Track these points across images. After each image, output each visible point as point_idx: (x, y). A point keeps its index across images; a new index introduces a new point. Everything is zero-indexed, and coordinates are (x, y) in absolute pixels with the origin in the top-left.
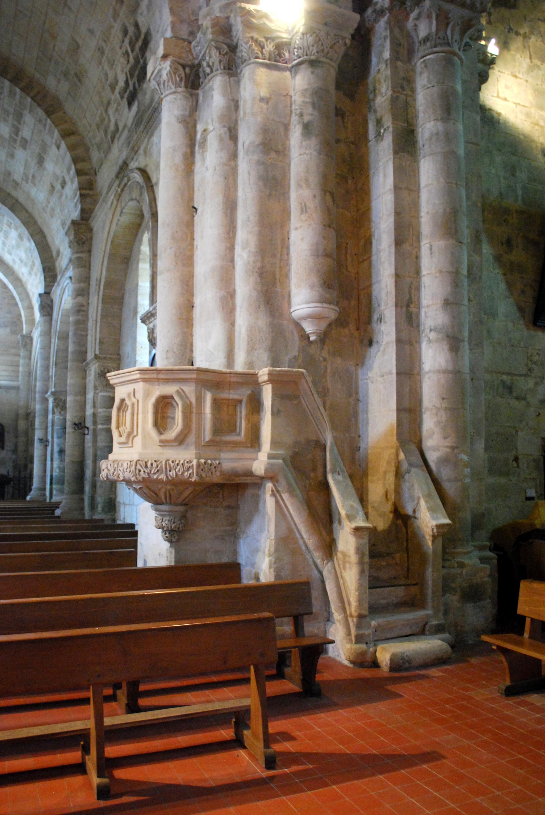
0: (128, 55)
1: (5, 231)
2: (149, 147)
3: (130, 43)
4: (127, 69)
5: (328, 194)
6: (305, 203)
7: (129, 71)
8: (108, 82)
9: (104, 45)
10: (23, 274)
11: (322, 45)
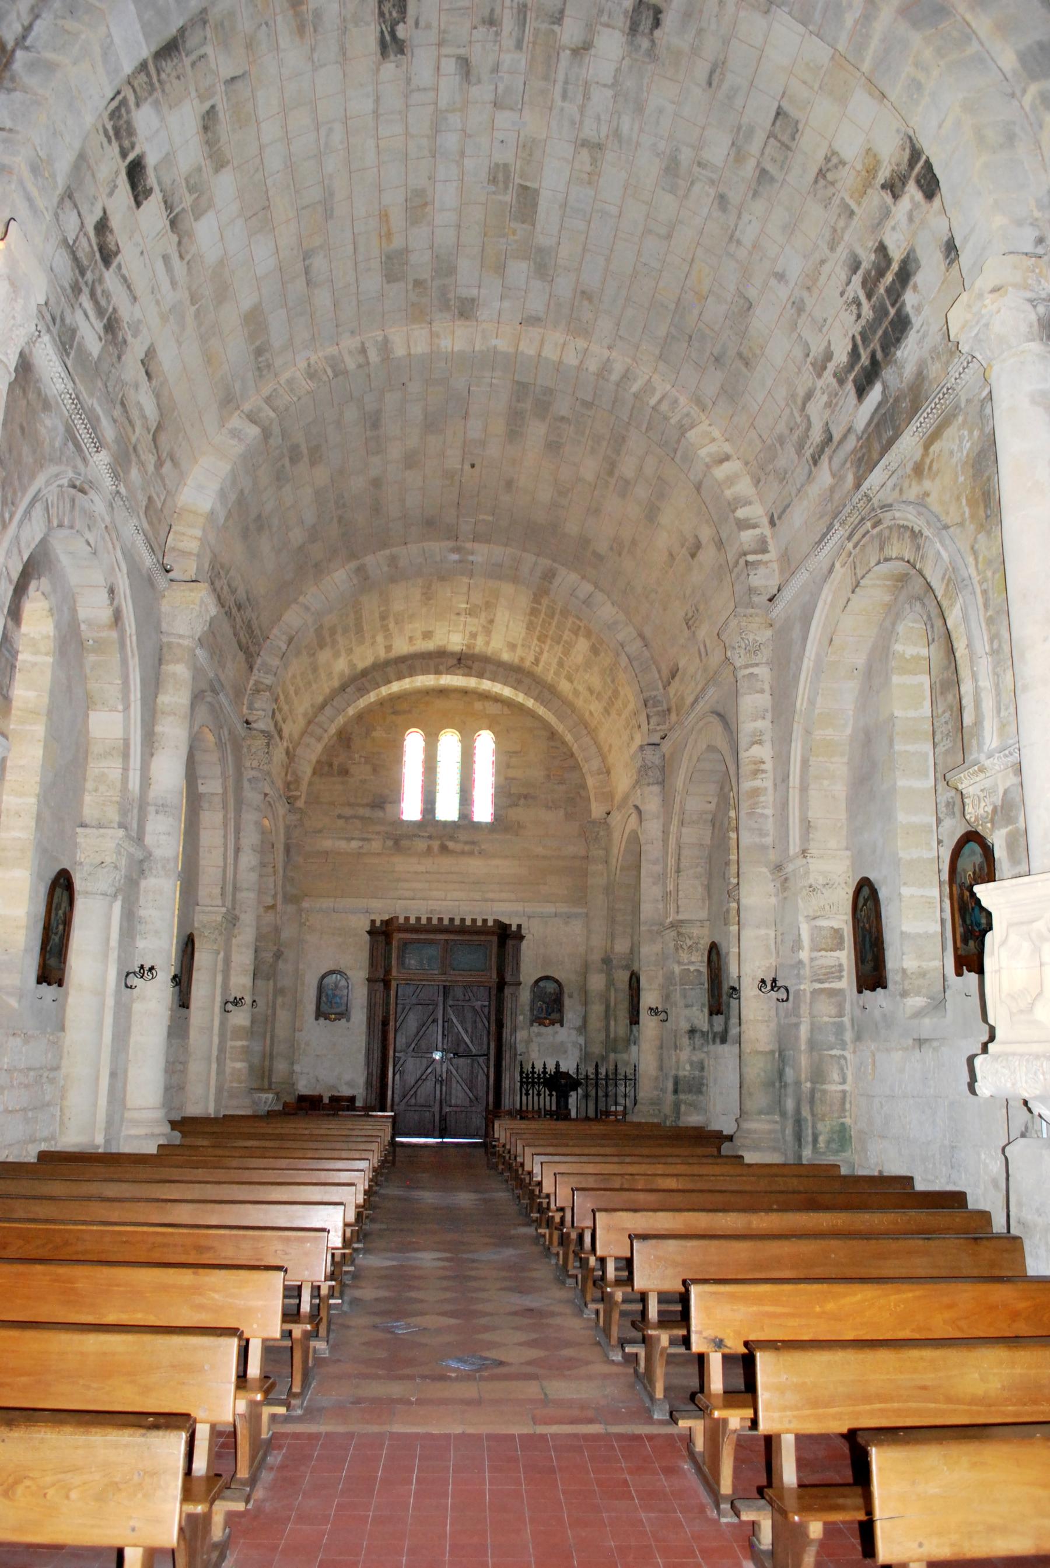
0: (859, 305)
1: (566, 642)
2: (928, 461)
3: (864, 284)
4: (856, 329)
7: (861, 333)
8: (809, 360)
9: (805, 294)
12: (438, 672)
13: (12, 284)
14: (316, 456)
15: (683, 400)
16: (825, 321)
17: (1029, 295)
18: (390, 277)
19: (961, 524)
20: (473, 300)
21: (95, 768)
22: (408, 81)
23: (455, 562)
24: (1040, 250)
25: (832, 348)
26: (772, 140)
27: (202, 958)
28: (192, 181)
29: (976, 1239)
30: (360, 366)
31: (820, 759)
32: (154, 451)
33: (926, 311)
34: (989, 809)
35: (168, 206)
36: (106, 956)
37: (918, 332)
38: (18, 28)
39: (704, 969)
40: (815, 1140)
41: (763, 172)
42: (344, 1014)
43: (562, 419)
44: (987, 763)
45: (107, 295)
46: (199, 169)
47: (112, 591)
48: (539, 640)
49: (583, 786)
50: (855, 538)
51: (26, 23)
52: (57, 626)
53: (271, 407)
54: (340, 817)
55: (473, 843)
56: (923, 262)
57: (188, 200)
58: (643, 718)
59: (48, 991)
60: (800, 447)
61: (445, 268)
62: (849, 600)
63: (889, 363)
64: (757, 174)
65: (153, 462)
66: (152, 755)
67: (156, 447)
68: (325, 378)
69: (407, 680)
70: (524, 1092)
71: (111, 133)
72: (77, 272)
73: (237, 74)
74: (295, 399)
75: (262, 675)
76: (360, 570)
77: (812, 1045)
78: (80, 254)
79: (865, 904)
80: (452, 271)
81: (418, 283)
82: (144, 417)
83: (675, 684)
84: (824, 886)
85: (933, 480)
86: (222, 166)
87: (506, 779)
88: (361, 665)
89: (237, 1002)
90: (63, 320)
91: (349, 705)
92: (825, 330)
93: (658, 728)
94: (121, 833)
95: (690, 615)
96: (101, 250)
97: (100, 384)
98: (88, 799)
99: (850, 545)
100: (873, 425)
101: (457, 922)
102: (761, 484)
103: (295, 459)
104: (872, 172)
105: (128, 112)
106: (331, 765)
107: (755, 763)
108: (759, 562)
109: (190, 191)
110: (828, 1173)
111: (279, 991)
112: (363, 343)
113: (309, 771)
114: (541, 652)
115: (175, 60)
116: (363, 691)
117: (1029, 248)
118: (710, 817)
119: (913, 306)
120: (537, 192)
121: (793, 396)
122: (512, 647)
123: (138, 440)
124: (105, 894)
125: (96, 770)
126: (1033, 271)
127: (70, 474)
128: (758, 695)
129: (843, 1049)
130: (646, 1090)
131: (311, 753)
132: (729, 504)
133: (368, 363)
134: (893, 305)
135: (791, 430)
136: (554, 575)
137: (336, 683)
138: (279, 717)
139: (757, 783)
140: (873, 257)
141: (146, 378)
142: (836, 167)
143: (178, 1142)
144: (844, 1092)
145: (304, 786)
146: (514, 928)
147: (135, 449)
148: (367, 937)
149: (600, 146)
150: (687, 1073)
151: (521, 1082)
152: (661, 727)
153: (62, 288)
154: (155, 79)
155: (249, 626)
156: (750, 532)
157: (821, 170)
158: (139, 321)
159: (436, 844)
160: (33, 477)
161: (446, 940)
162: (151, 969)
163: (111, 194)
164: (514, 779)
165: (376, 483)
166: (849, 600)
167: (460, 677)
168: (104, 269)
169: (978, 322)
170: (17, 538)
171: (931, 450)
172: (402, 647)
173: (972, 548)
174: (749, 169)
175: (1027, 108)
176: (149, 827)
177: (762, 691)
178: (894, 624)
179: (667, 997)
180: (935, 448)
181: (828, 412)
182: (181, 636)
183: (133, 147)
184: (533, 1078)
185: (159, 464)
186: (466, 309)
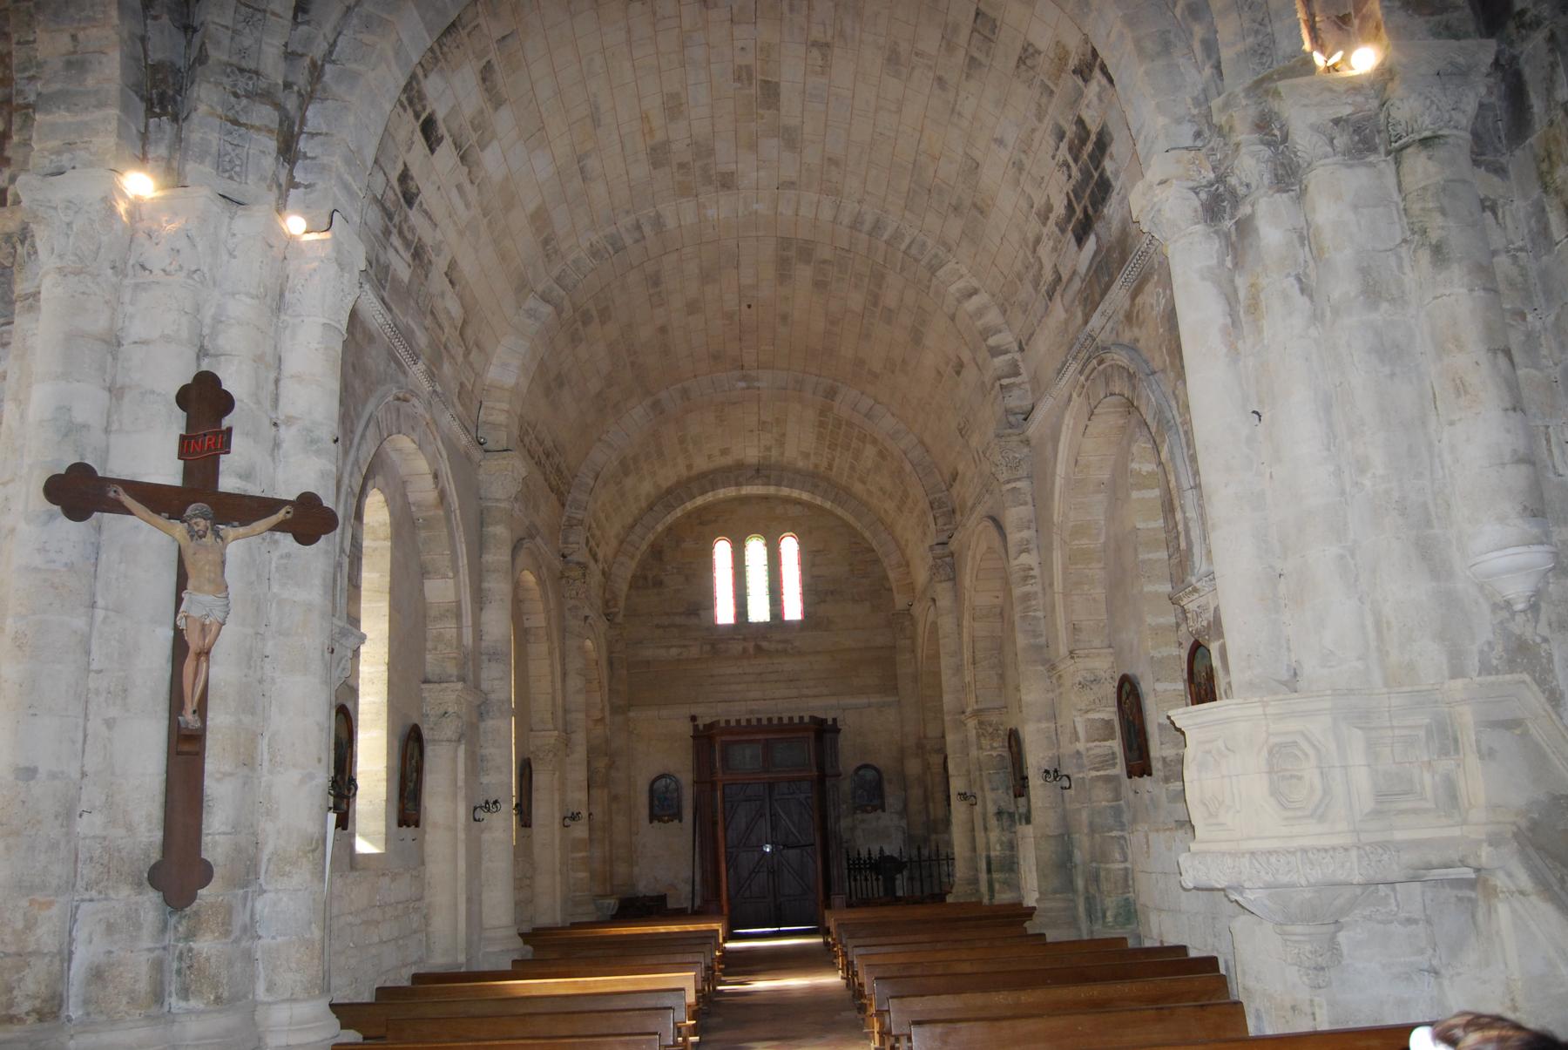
0: (1069, 167)
3: (1070, 149)
4: (1069, 187)
5: (1500, 356)
6: (1461, 378)
7: (1073, 191)
8: (1034, 210)
9: (1023, 156)
10: (886, 511)
11: (1438, 109)
12: (738, 484)
13: (339, 265)
14: (605, 315)
15: (930, 243)
16: (1042, 178)
17: (1192, 184)
18: (656, 164)
19: (1164, 371)
20: (733, 173)
21: (433, 629)
22: (654, 14)
23: (743, 389)
24: (1199, 143)
25: (1052, 201)
26: (975, 34)
27: (541, 779)
28: (476, 122)
29: (1202, 1006)
30: (637, 241)
31: (1079, 566)
32: (462, 344)
33: (1122, 176)
34: (1205, 623)
35: (457, 146)
36: (455, 796)
37: (1118, 194)
38: (325, 46)
39: (1006, 754)
40: (1104, 916)
41: (972, 59)
42: (678, 816)
43: (825, 262)
44: (1198, 585)
45: (412, 229)
46: (481, 112)
47: (436, 476)
48: (829, 448)
49: (886, 578)
50: (1087, 372)
51: (331, 41)
52: (392, 514)
53: (561, 286)
54: (658, 626)
55: (786, 641)
56: (1115, 136)
57: (474, 137)
58: (931, 518)
59: (408, 832)
60: (1036, 285)
61: (703, 150)
62: (1087, 426)
63: (1099, 218)
64: (967, 61)
65: (461, 353)
66: (481, 609)
67: (463, 339)
68: (607, 256)
69: (710, 494)
70: (852, 878)
71: (406, 103)
72: (386, 219)
73: (506, 33)
74: (582, 277)
75: (573, 510)
76: (656, 405)
77: (1093, 829)
78: (388, 205)
79: (1128, 698)
80: (711, 152)
81: (681, 166)
82: (451, 318)
83: (957, 485)
84: (1092, 682)
85: (1140, 328)
86: (501, 105)
87: (813, 577)
88: (665, 485)
89: (575, 817)
90: (378, 261)
91: (657, 523)
92: (1043, 185)
93: (945, 528)
94: (460, 685)
95: (962, 425)
96: (404, 196)
97: (412, 303)
98: (429, 657)
99: (1082, 378)
100: (1092, 272)
101: (775, 722)
102: (1008, 313)
103: (586, 319)
104: (1063, 58)
105: (418, 83)
106: (645, 578)
107: (1024, 571)
108: (1013, 384)
109: (475, 130)
110: (1115, 946)
111: (615, 798)
112: (638, 221)
113: (625, 587)
114: (834, 459)
115: (454, 35)
116: (670, 508)
117: (1189, 142)
118: (998, 610)
119: (1112, 172)
120: (777, 84)
121: (1025, 239)
122: (806, 456)
123: (448, 338)
124: (449, 741)
125: (434, 631)
126: (1194, 163)
127: (395, 391)
128: (1022, 507)
129: (1122, 830)
130: (960, 870)
131: (626, 569)
132: (981, 334)
133: (644, 237)
134: (1096, 169)
135: (1027, 268)
136: (835, 393)
137: (644, 504)
138: (592, 543)
139: (1027, 588)
140: (1074, 128)
141: (450, 286)
142: (1033, 55)
143: (529, 956)
144: (1126, 869)
145: (622, 603)
146: (830, 722)
147: (446, 347)
148: (691, 739)
149: (827, 45)
150: (998, 853)
151: (849, 869)
152: (948, 527)
153: (376, 236)
154: (438, 53)
155: (559, 470)
156: (1002, 358)
157: (1020, 58)
158: (441, 242)
159: (750, 646)
160: (364, 403)
161: (766, 740)
162: (496, 802)
163: (409, 149)
164: (819, 577)
165: (663, 330)
166: (1087, 426)
167: (760, 487)
168: (408, 210)
169: (1152, 209)
170: (357, 460)
171: (1136, 301)
172: (701, 464)
173: (1174, 393)
174: (960, 57)
175: (1179, 17)
176: (484, 675)
177: (1025, 503)
178: (1129, 445)
179: (970, 783)
180: (1139, 300)
181: (1055, 255)
182: (497, 500)
183: (424, 108)
184: (859, 863)
185: (467, 353)
186: (727, 182)
